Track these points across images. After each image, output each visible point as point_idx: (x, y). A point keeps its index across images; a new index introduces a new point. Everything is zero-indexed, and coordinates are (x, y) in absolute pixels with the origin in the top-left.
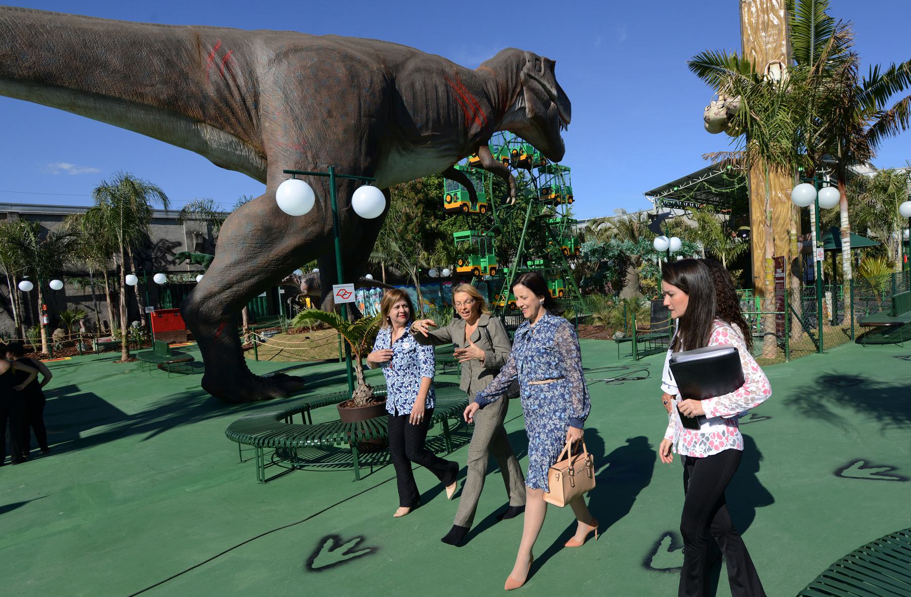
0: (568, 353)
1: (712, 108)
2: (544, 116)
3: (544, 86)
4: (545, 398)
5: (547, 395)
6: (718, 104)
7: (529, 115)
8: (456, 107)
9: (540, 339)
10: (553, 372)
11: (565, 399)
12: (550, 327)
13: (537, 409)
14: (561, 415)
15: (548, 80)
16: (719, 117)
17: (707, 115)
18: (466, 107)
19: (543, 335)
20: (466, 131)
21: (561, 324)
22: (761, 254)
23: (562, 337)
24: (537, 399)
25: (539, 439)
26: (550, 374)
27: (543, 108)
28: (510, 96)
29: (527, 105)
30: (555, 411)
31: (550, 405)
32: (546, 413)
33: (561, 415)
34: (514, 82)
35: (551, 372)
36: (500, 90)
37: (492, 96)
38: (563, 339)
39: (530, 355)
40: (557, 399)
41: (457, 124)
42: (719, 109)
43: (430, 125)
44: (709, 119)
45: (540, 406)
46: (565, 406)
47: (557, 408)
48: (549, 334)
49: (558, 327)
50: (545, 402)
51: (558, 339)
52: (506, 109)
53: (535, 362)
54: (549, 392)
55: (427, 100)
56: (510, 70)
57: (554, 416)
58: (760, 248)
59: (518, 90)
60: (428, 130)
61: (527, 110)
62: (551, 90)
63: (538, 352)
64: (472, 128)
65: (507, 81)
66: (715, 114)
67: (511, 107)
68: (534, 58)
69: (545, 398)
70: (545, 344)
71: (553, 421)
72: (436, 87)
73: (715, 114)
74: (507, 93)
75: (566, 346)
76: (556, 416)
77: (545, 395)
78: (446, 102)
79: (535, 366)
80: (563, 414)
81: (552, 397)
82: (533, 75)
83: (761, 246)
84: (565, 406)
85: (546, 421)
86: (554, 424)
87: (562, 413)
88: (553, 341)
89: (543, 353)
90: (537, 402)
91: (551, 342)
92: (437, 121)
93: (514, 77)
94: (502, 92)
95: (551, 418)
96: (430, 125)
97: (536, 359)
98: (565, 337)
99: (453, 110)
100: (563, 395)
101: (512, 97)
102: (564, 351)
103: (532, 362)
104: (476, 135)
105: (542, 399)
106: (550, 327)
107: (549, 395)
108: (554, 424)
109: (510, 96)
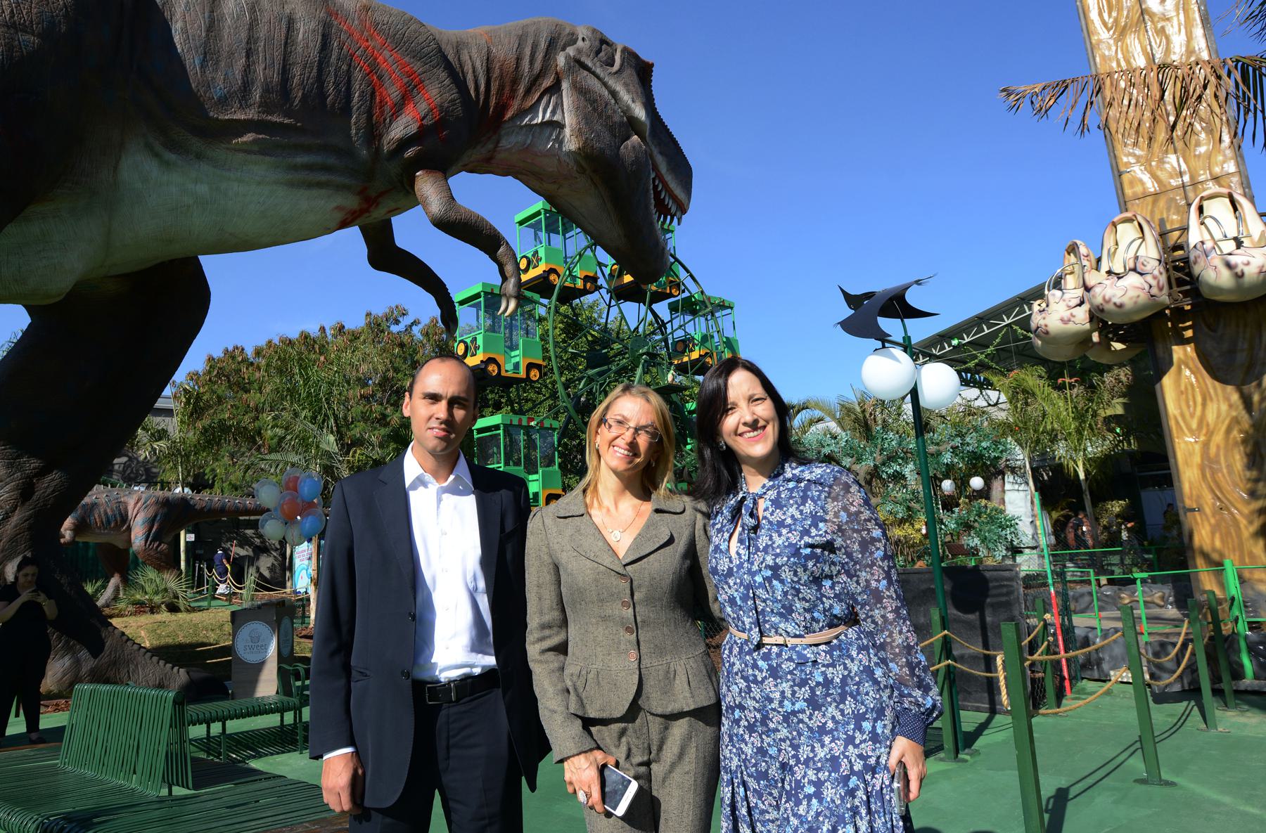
0: (863, 553)
1: (1053, 306)
2: (608, 152)
3: (614, 94)
4: (827, 683)
5: (829, 676)
6: (1066, 296)
7: (571, 143)
8: (349, 73)
9: (789, 521)
10: (831, 606)
11: (876, 682)
12: (807, 488)
13: (803, 711)
14: (874, 727)
15: (626, 85)
16: (1071, 327)
17: (1042, 322)
18: (380, 78)
19: (793, 510)
20: (373, 133)
21: (835, 478)
22: (1197, 448)
23: (845, 509)
24: (803, 683)
25: (821, 801)
26: (825, 610)
27: (606, 137)
28: (521, 90)
29: (569, 119)
30: (859, 718)
31: (843, 701)
32: (830, 725)
33: (874, 727)
34: (538, 65)
35: (827, 606)
36: (496, 73)
37: (470, 77)
38: (849, 515)
39: (771, 563)
40: (858, 684)
41: (346, 110)
42: (1070, 308)
43: (257, 95)
44: (1047, 333)
45: (814, 703)
46: (880, 700)
47: (863, 710)
48: (809, 507)
49: (830, 487)
50: (828, 695)
51: (836, 515)
52: (509, 114)
53: (782, 582)
54: (833, 665)
55: (252, 40)
56: (530, 42)
57: (857, 734)
58: (1190, 430)
59: (547, 82)
60: (249, 106)
61: (567, 131)
62: (633, 106)
63: (794, 555)
64: (394, 125)
65: (519, 60)
66: (1062, 320)
67: (522, 113)
68: (599, 36)
69: (827, 683)
70: (806, 532)
71: (856, 746)
72: (291, 22)
73: (1062, 320)
74: (515, 81)
75: (858, 531)
76: (862, 732)
77: (823, 673)
78: (314, 54)
79: (785, 594)
80: (879, 724)
81: (844, 679)
82: (590, 64)
83: (1194, 425)
84: (880, 700)
85: (838, 748)
86: (860, 756)
87: (875, 720)
88: (825, 521)
89: (807, 557)
90: (804, 692)
91: (821, 525)
92: (279, 94)
93: (540, 57)
94: (501, 76)
95: (850, 740)
96: (257, 95)
97: (787, 575)
98: (853, 509)
99: (336, 76)
100: (868, 671)
101: (528, 92)
102: (856, 547)
103: (775, 582)
104: (405, 143)
105: (818, 684)
106: (807, 488)
107: (837, 674)
108: (860, 756)
109: (521, 90)
